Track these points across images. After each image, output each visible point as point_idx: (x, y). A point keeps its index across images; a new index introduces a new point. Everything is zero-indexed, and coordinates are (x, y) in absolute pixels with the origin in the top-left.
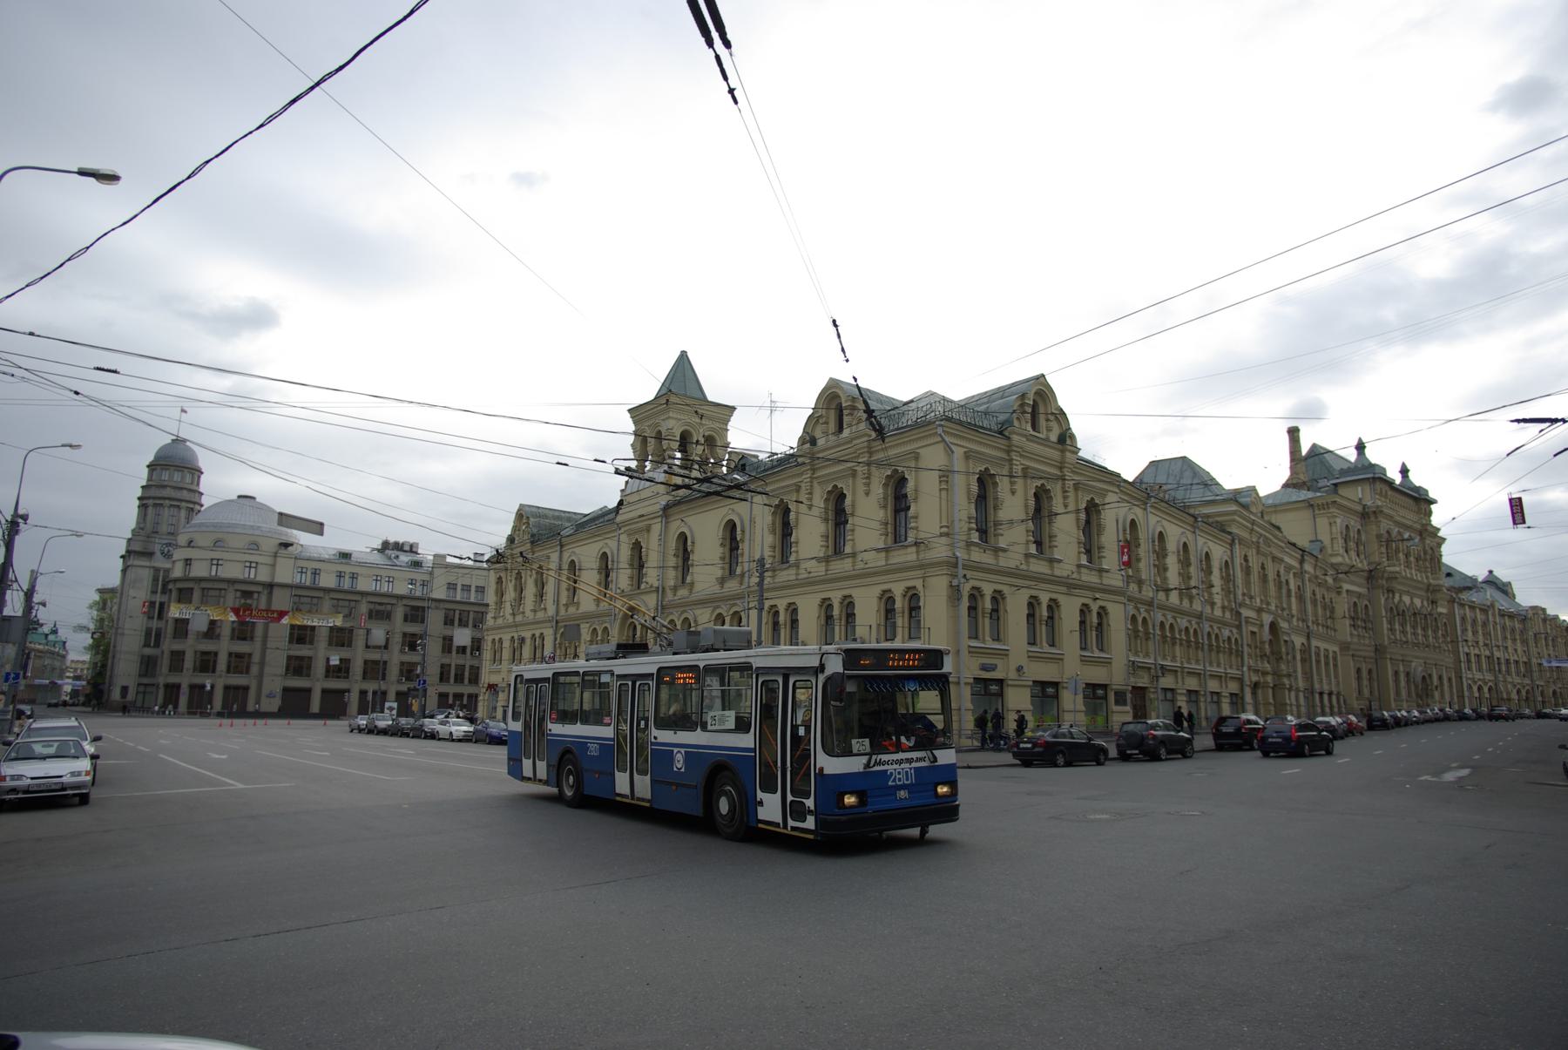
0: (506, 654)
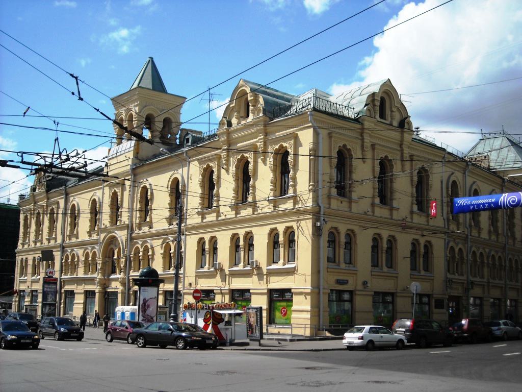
0: (30, 270)
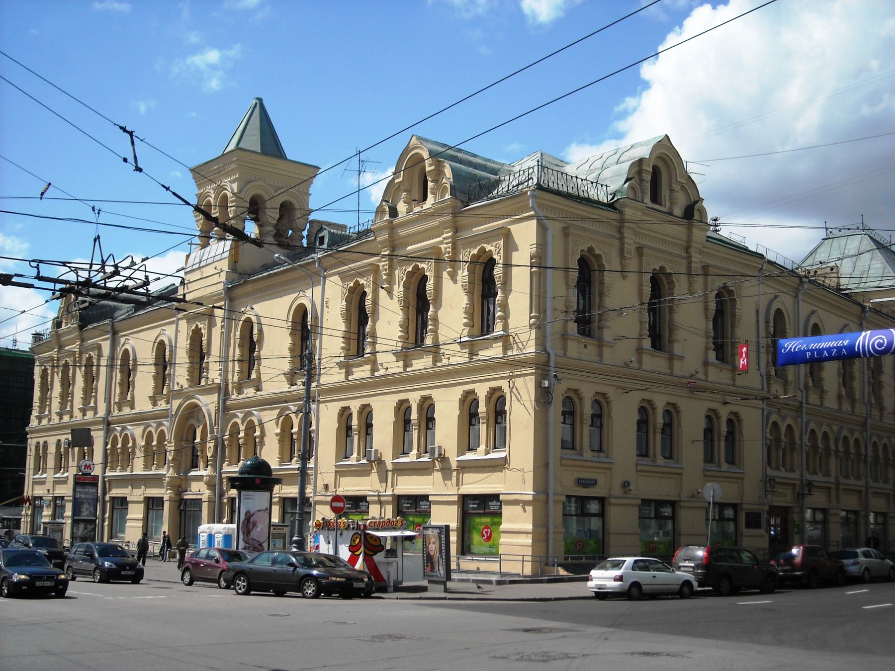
0: (51, 462)
